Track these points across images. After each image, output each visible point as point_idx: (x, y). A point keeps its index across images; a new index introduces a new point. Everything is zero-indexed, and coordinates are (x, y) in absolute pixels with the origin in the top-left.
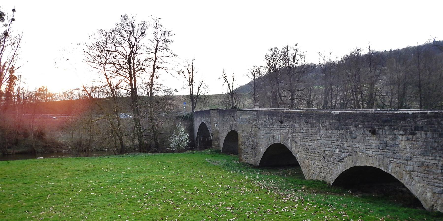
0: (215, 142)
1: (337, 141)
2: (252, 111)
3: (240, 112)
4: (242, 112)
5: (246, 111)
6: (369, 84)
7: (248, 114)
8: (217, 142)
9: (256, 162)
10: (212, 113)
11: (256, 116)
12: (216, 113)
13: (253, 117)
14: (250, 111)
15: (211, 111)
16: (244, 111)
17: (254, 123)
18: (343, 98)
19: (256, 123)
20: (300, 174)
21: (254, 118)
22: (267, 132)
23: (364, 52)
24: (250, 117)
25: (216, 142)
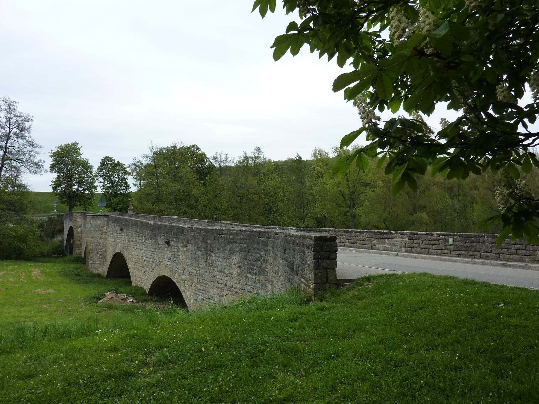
0: (76, 250)
1: (151, 251)
2: (102, 217)
3: (90, 217)
4: (92, 217)
5: (96, 217)
6: (479, 132)
7: (99, 219)
8: (79, 250)
9: (104, 272)
10: (76, 216)
11: (107, 222)
12: (80, 216)
13: (104, 223)
14: (100, 217)
15: (74, 213)
16: (94, 217)
17: (105, 230)
18: (204, 354)
19: (107, 230)
20: (130, 283)
21: (105, 224)
22: (113, 240)
23: (179, 146)
24: (100, 223)
25: (78, 250)
